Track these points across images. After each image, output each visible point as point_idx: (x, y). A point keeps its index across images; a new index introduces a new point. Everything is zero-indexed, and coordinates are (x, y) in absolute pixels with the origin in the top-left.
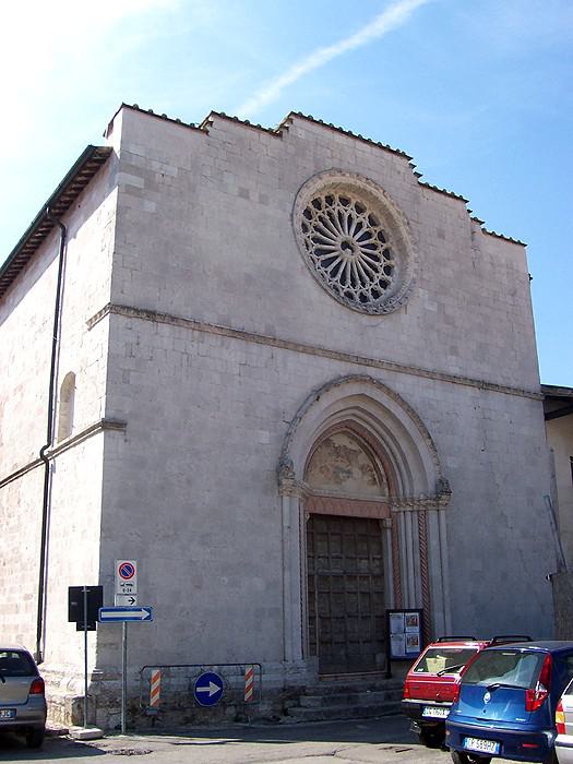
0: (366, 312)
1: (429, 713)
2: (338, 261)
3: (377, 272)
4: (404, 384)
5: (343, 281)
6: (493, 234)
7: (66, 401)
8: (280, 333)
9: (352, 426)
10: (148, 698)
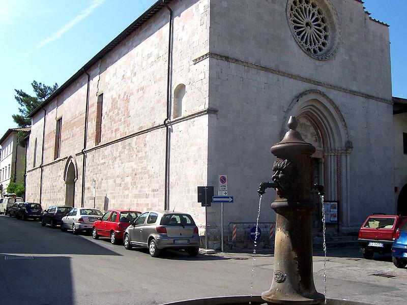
0: (318, 59)
1: (371, 244)
2: (302, 29)
3: (321, 38)
4: (333, 94)
5: (306, 43)
6: (374, 20)
7: (176, 98)
8: (281, 68)
9: (309, 114)
10: (231, 237)
